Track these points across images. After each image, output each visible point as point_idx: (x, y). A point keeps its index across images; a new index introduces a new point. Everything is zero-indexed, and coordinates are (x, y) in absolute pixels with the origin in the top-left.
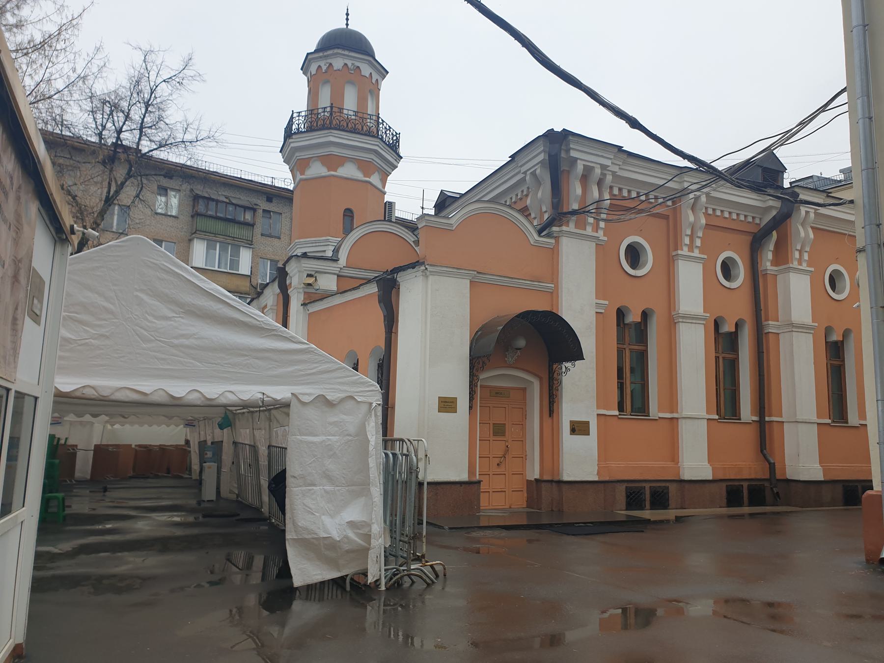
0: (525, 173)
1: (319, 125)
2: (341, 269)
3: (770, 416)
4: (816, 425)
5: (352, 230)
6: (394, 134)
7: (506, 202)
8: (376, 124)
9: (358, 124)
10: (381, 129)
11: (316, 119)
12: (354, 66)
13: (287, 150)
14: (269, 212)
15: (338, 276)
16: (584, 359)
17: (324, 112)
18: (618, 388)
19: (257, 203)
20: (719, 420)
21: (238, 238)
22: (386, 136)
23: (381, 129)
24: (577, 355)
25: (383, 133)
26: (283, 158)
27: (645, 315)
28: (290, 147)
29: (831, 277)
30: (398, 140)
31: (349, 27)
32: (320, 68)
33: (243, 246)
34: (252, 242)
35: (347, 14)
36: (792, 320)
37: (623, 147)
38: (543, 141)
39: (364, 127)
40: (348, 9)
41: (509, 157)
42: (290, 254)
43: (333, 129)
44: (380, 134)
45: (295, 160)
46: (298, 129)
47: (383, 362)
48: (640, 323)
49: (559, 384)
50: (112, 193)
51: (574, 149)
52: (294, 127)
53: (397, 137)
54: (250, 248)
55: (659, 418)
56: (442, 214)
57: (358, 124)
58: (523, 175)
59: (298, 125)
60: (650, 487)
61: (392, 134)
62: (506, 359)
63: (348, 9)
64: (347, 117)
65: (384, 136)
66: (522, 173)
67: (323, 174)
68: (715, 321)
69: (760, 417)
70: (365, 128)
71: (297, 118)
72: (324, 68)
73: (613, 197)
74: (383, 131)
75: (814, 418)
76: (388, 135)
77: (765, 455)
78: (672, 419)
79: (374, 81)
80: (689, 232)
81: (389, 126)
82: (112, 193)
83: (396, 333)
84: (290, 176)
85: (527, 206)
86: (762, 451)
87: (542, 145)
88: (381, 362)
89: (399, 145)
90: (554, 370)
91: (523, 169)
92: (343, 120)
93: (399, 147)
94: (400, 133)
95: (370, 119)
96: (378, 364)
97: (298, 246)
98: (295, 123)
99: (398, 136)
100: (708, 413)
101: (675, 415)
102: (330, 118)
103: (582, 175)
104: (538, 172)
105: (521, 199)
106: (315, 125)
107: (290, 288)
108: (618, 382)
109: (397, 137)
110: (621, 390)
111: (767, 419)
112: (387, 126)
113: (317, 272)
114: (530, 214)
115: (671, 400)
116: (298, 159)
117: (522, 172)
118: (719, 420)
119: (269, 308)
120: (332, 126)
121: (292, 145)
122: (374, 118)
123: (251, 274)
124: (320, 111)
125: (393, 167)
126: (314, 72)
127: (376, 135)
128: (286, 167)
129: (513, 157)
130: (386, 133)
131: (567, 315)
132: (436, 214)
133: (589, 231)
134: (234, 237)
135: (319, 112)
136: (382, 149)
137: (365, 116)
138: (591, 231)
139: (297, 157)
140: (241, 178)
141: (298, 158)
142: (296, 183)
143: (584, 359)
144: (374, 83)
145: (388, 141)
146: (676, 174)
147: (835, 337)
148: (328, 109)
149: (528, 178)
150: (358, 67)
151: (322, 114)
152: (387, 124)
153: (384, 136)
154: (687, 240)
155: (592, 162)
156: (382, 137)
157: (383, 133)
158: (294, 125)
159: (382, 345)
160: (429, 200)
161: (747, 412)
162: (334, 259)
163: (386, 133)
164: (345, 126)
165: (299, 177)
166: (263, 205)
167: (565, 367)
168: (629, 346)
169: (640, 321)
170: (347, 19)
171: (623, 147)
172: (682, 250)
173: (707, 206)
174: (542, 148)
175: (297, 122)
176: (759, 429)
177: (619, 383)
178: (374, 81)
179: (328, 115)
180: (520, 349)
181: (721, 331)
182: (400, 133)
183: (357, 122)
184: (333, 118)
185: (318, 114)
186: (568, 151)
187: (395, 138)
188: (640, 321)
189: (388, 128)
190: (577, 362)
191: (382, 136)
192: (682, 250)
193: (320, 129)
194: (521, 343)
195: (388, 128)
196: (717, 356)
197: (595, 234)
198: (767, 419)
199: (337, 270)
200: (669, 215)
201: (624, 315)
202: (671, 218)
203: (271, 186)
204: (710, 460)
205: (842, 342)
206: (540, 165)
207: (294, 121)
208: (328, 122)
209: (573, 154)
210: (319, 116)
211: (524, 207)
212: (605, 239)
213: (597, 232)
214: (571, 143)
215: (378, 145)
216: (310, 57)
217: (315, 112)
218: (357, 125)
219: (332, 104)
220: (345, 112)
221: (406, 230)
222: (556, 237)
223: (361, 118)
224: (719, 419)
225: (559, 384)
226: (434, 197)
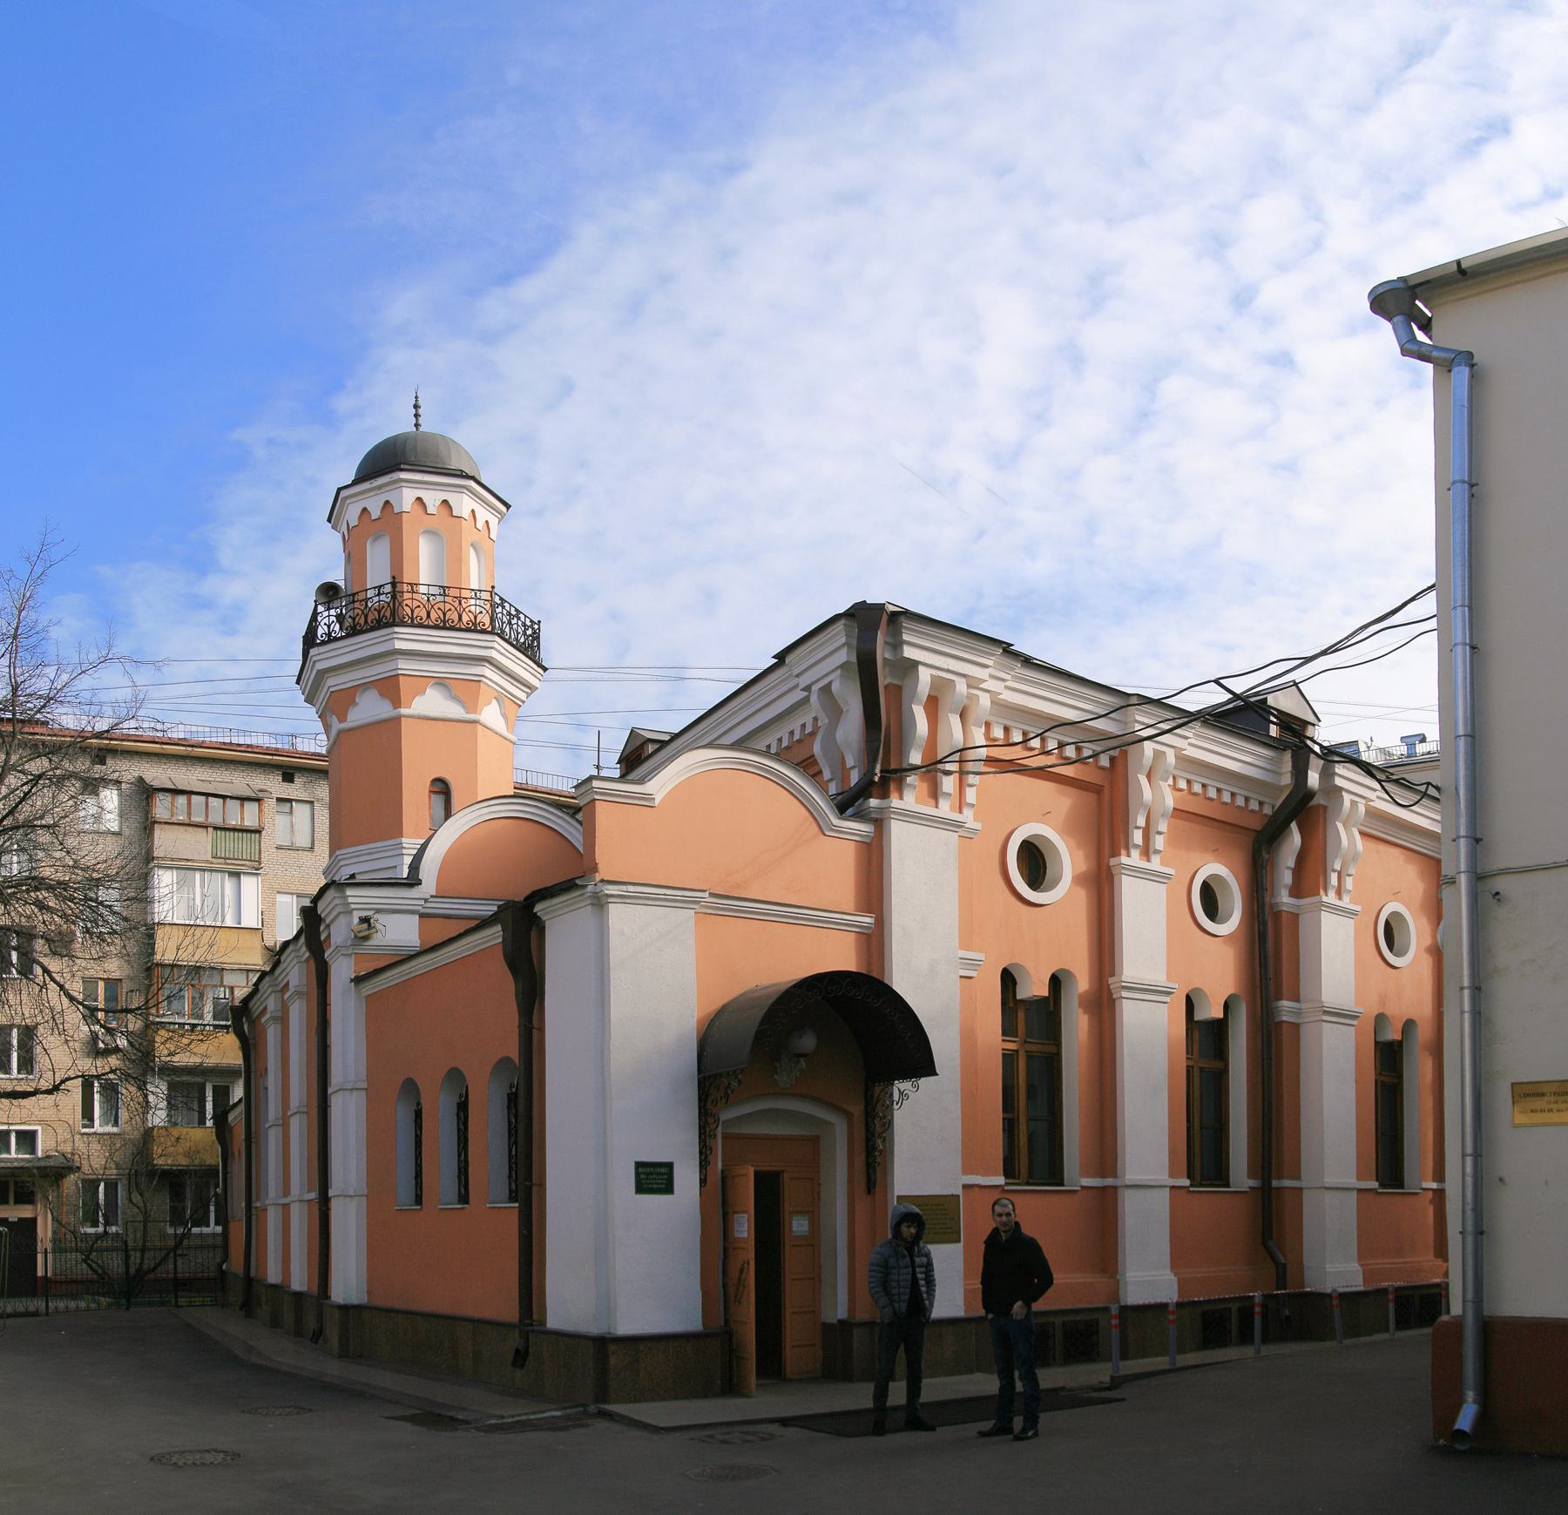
0: (808, 688)
1: (369, 622)
2: (426, 901)
3: (1280, 1177)
4: (1355, 1192)
5: (448, 814)
6: (528, 623)
7: (769, 747)
8: (488, 607)
10: (500, 615)
11: (363, 611)
13: (310, 676)
15: (422, 916)
16: (937, 1075)
17: (379, 594)
18: (1004, 1131)
19: (265, 788)
20: (1191, 1189)
21: (234, 859)
22: (511, 629)
23: (500, 615)
24: (920, 1062)
25: (503, 623)
27: (1056, 982)
28: (314, 672)
29: (1387, 924)
30: (536, 636)
31: (421, 429)
32: (366, 513)
33: (244, 873)
34: (260, 863)
35: (416, 407)
36: (1323, 999)
37: (1012, 645)
38: (845, 625)
40: (416, 397)
41: (774, 657)
44: (497, 625)
45: (326, 693)
46: (329, 634)
47: (517, 1090)
48: (1045, 999)
49: (887, 1125)
51: (909, 644)
52: (320, 631)
53: (533, 629)
54: (257, 874)
55: (1083, 1187)
56: (631, 777)
58: (805, 694)
59: (329, 627)
60: (1064, 1322)
61: (524, 624)
62: (776, 1077)
63: (416, 397)
64: (426, 598)
65: (507, 630)
66: (803, 690)
67: (384, 716)
68: (1188, 997)
69: (1263, 1182)
70: (465, 618)
71: (326, 614)
72: (375, 513)
73: (992, 743)
74: (505, 619)
75: (1352, 1181)
76: (515, 626)
77: (246, 1141)
78: (1104, 1188)
80: (1141, 822)
81: (516, 610)
83: (542, 1030)
84: (319, 727)
85: (814, 756)
86: (1264, 1244)
87: (844, 633)
88: (514, 1090)
89: (538, 646)
90: (876, 1095)
91: (804, 681)
92: (419, 606)
93: (539, 649)
94: (539, 622)
95: (476, 598)
96: (508, 1094)
97: (342, 863)
98: (322, 624)
99: (536, 627)
100: (1172, 1175)
101: (1109, 1181)
102: (391, 605)
103: (929, 695)
104: (835, 687)
105: (799, 741)
106: (362, 621)
107: (328, 948)
108: (1004, 1119)
109: (533, 629)
110: (1009, 1134)
111: (1275, 1183)
112: (513, 609)
113: (378, 911)
114: (820, 772)
115: (1105, 1153)
116: (332, 692)
117: (802, 686)
118: (1191, 1189)
119: (294, 990)
121: (320, 666)
122: (486, 596)
123: (263, 926)
124: (370, 594)
125: (529, 688)
126: (354, 522)
127: (490, 629)
128: (311, 712)
129: (781, 657)
130: (510, 623)
131: (901, 983)
132: (623, 777)
133: (945, 809)
134: (225, 859)
135: (368, 596)
136: (502, 654)
137: (465, 594)
138: (948, 809)
139: (329, 687)
140: (231, 743)
141: (332, 689)
142: (331, 740)
143: (937, 1075)
145: (517, 640)
146: (1118, 706)
147: (1393, 1034)
148: (388, 589)
149: (814, 698)
151: (376, 599)
152: (511, 605)
153: (507, 630)
154: (1138, 837)
155: (948, 671)
156: (503, 631)
157: (503, 623)
159: (514, 1052)
160: (608, 750)
161: (1240, 1172)
162: (413, 881)
163: (510, 623)
164: (425, 617)
165: (337, 726)
166: (274, 785)
167: (899, 1090)
168: (1026, 1045)
169: (1047, 995)
170: (417, 416)
171: (1012, 645)
172: (1129, 856)
173: (1177, 773)
174: (843, 640)
175: (326, 621)
177: (1006, 1121)
178: (480, 524)
179: (388, 600)
180: (804, 1055)
181: (1197, 1018)
182: (539, 622)
183: (448, 607)
184: (397, 604)
185: (366, 600)
186: (897, 645)
187: (529, 632)
188: (1047, 995)
189: (513, 612)
190: (923, 1081)
191: (501, 629)
192: (1129, 856)
193: (373, 629)
194: (808, 1042)
195: (513, 612)
196: (1190, 1064)
197: (956, 816)
198: (1275, 1183)
199: (419, 905)
200: (1103, 786)
201: (1014, 983)
202: (1106, 791)
204: (1175, 1265)
205: (1400, 1043)
206: (839, 672)
207: (319, 619)
208: (388, 614)
209: (909, 652)
210: (370, 605)
211: (808, 759)
212: (978, 826)
213: (961, 812)
214: (903, 631)
216: (343, 494)
217: (361, 596)
218: (449, 613)
219: (394, 578)
220: (423, 589)
221: (559, 813)
222: (876, 820)
223: (456, 598)
224: (1192, 1185)
225: (887, 1125)
226: (616, 744)
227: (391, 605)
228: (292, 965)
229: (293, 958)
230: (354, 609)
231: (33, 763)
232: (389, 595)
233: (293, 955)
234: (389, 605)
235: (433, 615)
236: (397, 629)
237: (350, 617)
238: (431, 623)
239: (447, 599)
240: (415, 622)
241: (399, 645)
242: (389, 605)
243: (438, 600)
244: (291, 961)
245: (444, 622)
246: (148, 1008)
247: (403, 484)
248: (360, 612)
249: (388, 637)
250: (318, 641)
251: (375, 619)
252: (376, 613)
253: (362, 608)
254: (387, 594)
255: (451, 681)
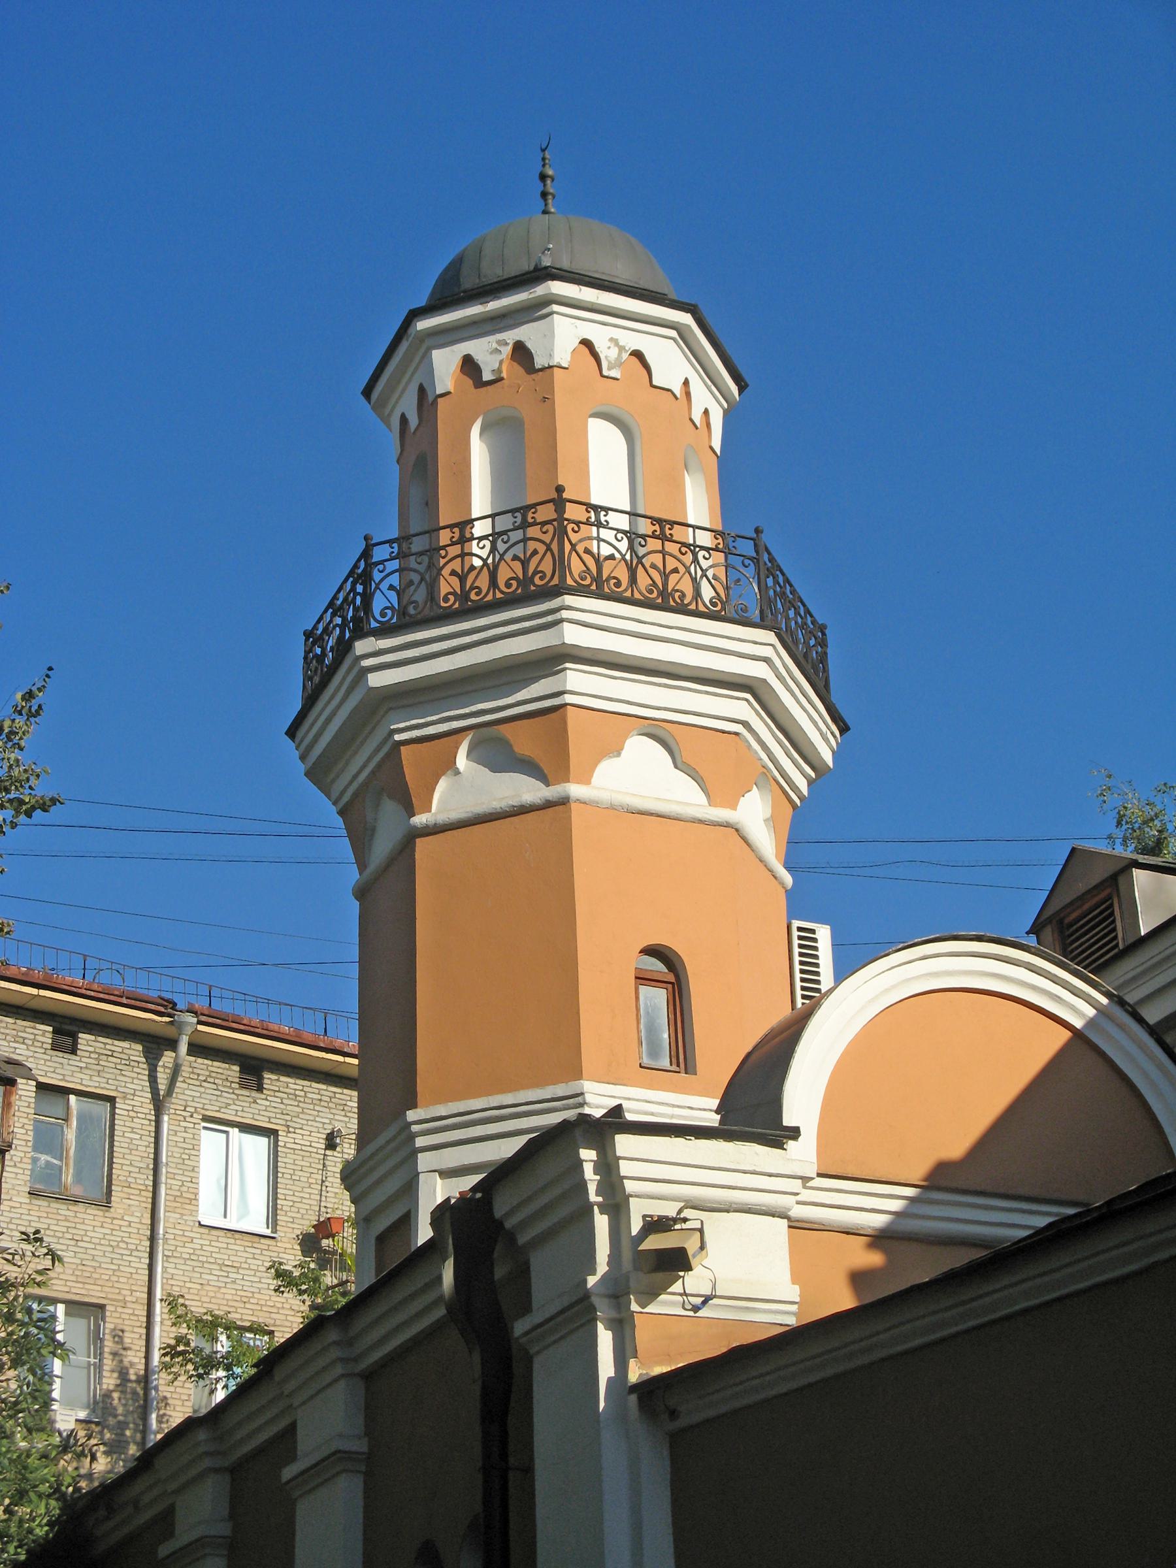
1: (501, 583)
9: (676, 571)
12: (622, 349)
14: (64, 1091)
26: (303, 758)
27: (785, 1150)
39: (704, 582)
42: (59, 1247)
43: (572, 591)
46: (464, 596)
50: (497, 560)
57: (676, 571)
79: (697, 416)
82: (497, 560)
98: (384, 586)
102: (555, 547)
120: (570, 582)
144: (698, 422)
150: (638, 355)
158: (378, 594)
176: (40, 1010)
183: (671, 563)
184: (567, 547)
190: (690, 1272)
203: (1171, 1049)
207: (377, 576)
208: (547, 566)
215: (766, 660)
218: (673, 578)
227: (555, 547)
228: (327, 1378)
229: (333, 1363)
230: (525, 540)
231: (104, 1380)
232: (550, 528)
233: (335, 1353)
234: (549, 548)
235: (643, 581)
236: (569, 600)
237: (453, 573)
238: (637, 596)
239: (671, 547)
240: (606, 590)
241: (573, 635)
242: (549, 548)
243: (649, 548)
244: (324, 1369)
245: (663, 593)
246: (19, 1386)
247: (555, 308)
248: (541, 548)
249: (550, 618)
250: (374, 624)
251: (516, 579)
252: (517, 566)
253: (421, 568)
254: (544, 524)
255: (503, 728)
